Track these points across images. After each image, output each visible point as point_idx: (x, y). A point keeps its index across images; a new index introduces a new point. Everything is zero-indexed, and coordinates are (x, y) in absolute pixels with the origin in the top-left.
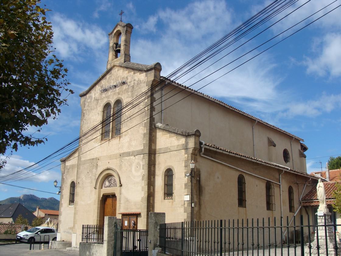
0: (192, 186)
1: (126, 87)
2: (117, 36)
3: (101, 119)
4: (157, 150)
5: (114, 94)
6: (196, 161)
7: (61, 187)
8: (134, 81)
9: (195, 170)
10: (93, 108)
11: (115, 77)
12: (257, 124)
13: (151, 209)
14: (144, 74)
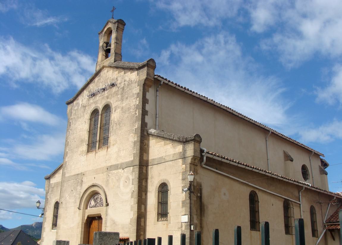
0: (191, 204)
1: (115, 89)
2: (108, 34)
3: (87, 127)
4: (150, 161)
5: (103, 98)
6: (195, 172)
7: (44, 208)
8: (124, 82)
9: (195, 184)
10: (80, 116)
11: (104, 79)
12: (271, 135)
13: (142, 233)
14: (136, 73)
